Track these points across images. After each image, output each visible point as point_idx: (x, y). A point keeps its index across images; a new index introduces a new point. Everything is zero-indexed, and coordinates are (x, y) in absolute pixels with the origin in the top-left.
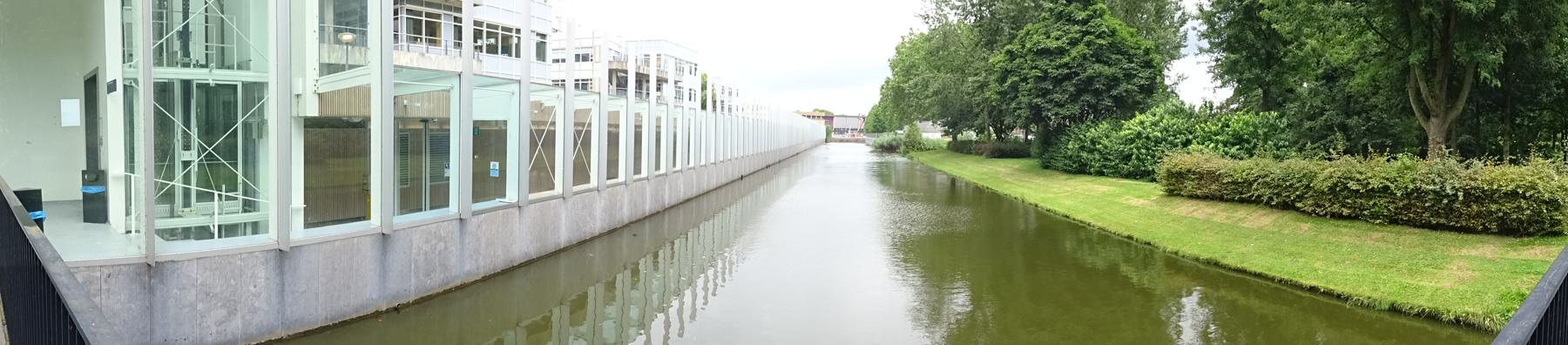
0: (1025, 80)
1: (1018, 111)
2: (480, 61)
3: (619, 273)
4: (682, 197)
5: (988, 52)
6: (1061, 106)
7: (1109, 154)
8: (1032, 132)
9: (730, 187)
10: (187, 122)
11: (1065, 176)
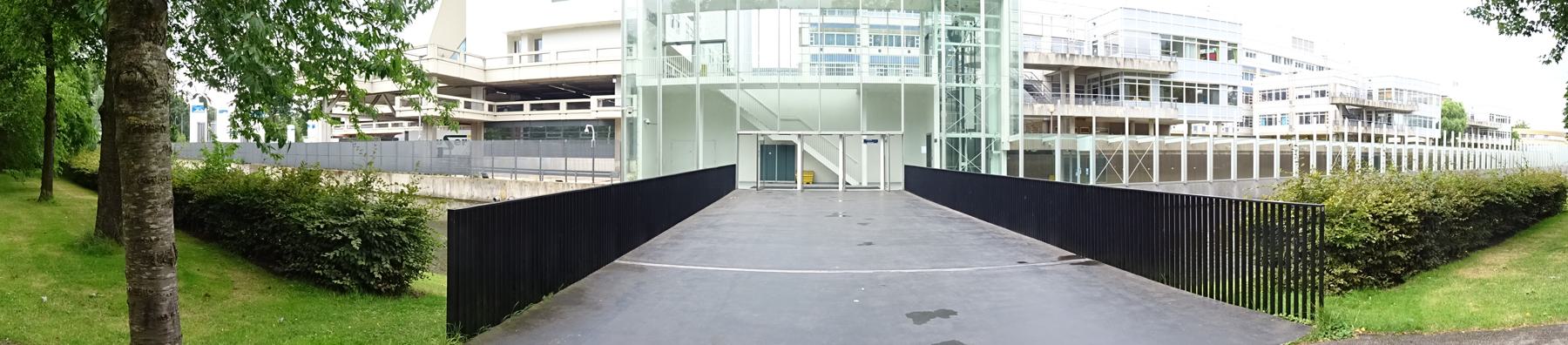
2: (1176, 109)
10: (963, 153)
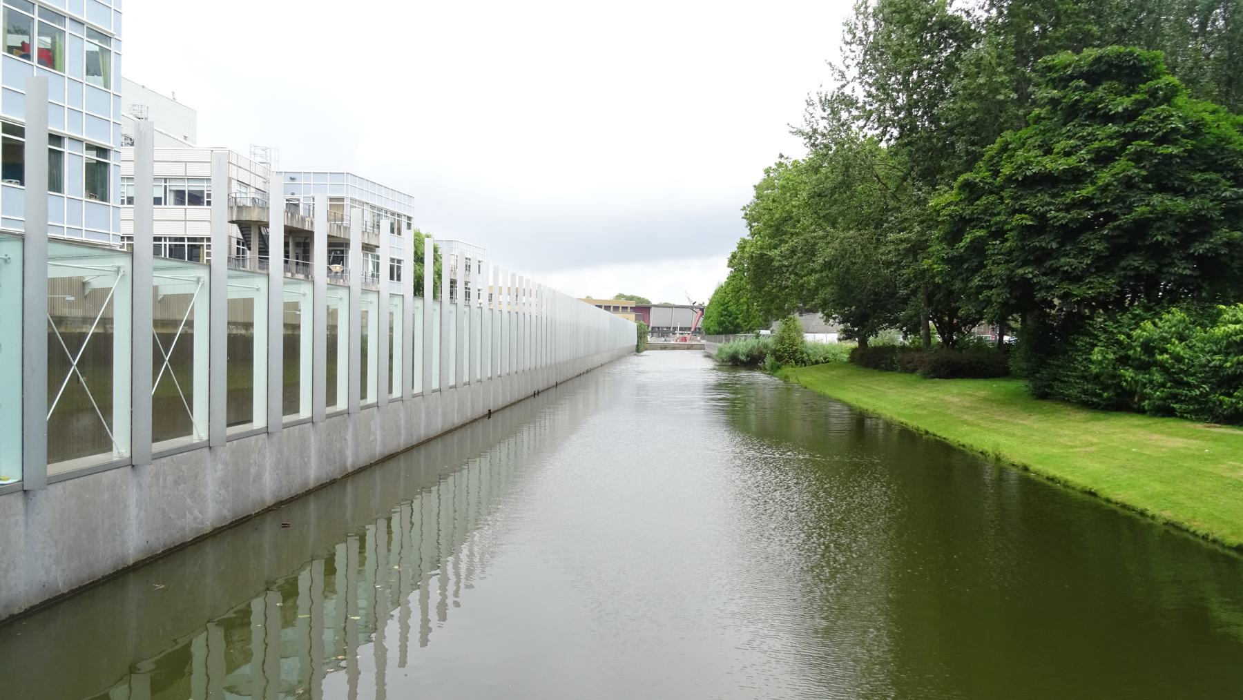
0: (999, 233)
1: (985, 293)
3: (257, 596)
4: (379, 450)
5: (925, 189)
6: (1076, 279)
7: (1187, 373)
8: (1013, 330)
9: (469, 430)
11: (1083, 415)
